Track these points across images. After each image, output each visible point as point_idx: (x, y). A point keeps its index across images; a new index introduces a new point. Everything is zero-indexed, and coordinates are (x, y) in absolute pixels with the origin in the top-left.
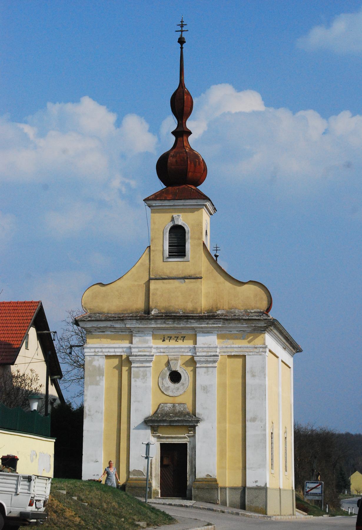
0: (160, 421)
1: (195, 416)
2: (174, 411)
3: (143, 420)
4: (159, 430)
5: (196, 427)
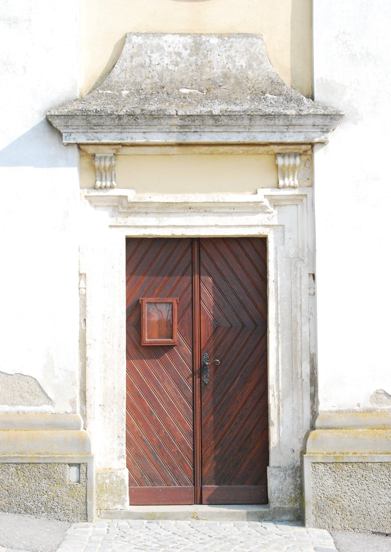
0: (121, 121)
1: (312, 97)
2: (200, 68)
3: (38, 119)
4: (125, 166)
5: (319, 154)
